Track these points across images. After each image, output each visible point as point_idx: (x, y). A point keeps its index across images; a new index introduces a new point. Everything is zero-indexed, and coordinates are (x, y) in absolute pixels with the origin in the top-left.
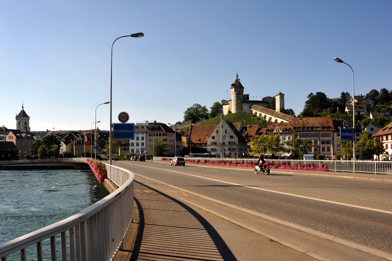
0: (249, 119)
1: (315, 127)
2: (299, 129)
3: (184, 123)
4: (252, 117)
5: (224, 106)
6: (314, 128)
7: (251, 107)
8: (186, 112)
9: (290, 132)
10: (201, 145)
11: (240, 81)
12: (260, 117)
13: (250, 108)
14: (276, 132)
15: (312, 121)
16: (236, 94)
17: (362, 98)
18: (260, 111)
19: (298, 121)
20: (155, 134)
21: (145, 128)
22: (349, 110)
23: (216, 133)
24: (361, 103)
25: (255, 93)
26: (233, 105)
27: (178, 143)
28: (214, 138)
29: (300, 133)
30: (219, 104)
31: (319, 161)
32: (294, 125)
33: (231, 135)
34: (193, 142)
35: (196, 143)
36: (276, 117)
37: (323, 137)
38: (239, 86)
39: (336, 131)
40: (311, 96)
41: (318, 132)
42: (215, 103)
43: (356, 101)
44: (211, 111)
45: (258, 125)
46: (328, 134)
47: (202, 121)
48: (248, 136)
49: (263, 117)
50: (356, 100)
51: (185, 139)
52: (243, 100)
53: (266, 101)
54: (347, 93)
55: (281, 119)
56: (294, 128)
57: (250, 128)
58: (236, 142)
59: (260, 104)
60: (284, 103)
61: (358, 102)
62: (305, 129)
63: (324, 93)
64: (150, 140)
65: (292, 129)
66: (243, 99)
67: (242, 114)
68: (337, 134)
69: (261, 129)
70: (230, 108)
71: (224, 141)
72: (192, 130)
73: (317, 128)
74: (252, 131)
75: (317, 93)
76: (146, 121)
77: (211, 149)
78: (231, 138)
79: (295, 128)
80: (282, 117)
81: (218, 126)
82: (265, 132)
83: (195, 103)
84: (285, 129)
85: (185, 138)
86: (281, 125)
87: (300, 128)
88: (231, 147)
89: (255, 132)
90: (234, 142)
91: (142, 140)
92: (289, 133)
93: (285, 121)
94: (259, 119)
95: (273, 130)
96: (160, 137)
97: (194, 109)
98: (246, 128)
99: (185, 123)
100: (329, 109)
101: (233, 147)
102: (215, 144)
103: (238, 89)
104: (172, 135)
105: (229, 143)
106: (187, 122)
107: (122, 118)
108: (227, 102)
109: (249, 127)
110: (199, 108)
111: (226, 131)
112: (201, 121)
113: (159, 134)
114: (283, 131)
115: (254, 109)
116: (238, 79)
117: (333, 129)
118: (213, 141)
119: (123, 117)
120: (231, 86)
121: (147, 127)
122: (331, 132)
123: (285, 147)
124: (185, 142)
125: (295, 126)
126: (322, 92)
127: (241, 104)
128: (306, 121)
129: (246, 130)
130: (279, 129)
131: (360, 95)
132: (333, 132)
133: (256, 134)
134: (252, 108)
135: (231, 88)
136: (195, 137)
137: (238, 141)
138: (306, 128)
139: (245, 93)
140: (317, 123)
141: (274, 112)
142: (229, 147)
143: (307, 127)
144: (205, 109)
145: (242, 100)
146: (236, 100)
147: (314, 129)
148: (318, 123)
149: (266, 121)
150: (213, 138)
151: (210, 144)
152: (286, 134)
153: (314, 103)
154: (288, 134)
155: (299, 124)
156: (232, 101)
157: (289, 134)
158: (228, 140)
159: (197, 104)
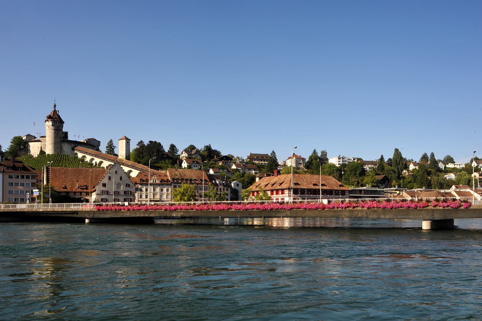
4: (81, 162)
5: (31, 144)
6: (193, 180)
13: (73, 149)
14: (152, 182)
16: (54, 130)
18: (93, 156)
23: (108, 180)
25: (76, 132)
29: (179, 185)
33: (126, 183)
35: (61, 191)
43: (187, 155)
50: (186, 153)
52: (63, 139)
60: (130, 150)
66: (61, 137)
71: (118, 190)
73: (195, 181)
77: (101, 199)
79: (174, 179)
80: (131, 166)
88: (128, 197)
90: (131, 192)
92: (168, 185)
96: (23, 179)
101: (129, 197)
103: (57, 123)
105: (125, 192)
111: (121, 178)
113: (27, 176)
114: (160, 182)
118: (104, 189)
123: (163, 200)
127: (61, 143)
130: (156, 180)
134: (76, 150)
139: (64, 130)
141: (117, 158)
142: (125, 197)
143: (186, 179)
146: (54, 137)
147: (193, 182)
150: (104, 185)
152: (165, 185)
154: (167, 185)
155: (176, 175)
157: (168, 185)
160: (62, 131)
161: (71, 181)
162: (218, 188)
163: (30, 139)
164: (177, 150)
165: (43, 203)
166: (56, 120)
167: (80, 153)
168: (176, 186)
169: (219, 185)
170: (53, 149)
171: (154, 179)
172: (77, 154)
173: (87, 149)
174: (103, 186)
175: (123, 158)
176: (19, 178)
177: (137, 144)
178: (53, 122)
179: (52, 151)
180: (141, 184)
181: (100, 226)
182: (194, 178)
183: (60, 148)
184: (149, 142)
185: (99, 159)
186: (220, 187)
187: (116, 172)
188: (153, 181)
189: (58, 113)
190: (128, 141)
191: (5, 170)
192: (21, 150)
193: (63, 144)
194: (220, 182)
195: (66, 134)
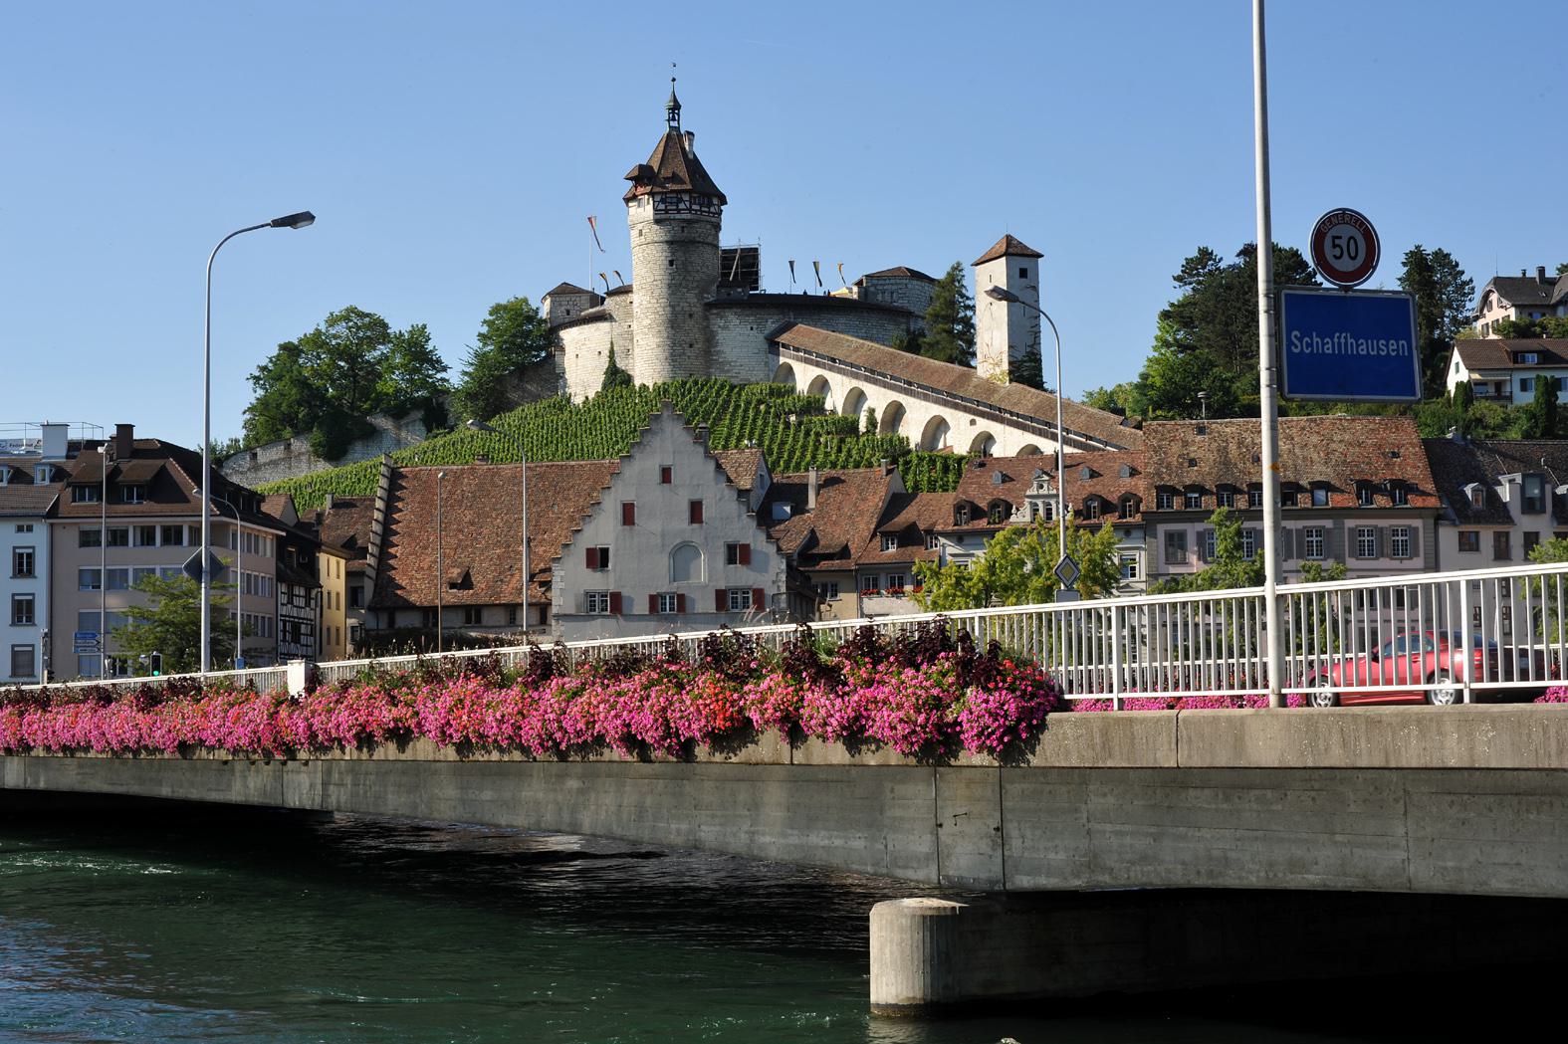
0: (775, 433)
1: (1304, 482)
3: (255, 456)
5: (568, 336)
6: (1300, 489)
8: (263, 369)
9: (1129, 519)
10: (479, 620)
11: (694, 149)
12: (851, 417)
13: (773, 346)
14: (1028, 519)
16: (665, 247)
17: (1549, 295)
18: (856, 376)
19: (1186, 444)
20: (131, 525)
21: (42, 479)
22: (1476, 376)
23: (620, 528)
24: (1544, 328)
26: (647, 322)
27: (296, 601)
30: (531, 317)
31: (1454, 586)
33: (730, 540)
34: (413, 598)
36: (977, 419)
38: (689, 187)
39: (1454, 517)
40: (1198, 275)
41: (1328, 524)
42: (497, 310)
43: (1512, 314)
44: (470, 369)
45: (889, 472)
46: (1395, 533)
47: (398, 443)
48: (815, 551)
49: (879, 416)
50: (1505, 302)
51: (338, 577)
53: (887, 297)
54: (1442, 257)
55: (1020, 432)
56: (1160, 489)
57: (830, 492)
58: (770, 591)
61: (1527, 319)
64: (88, 579)
65: (1149, 503)
66: (715, 284)
67: (718, 395)
68: (1461, 534)
69: (914, 496)
70: (619, 348)
72: (400, 505)
73: (1321, 494)
76: (46, 426)
78: (731, 560)
79: (1165, 492)
80: (1032, 419)
81: (631, 471)
82: (944, 520)
83: (338, 308)
84: (1092, 497)
85: (338, 563)
87: (1202, 490)
89: (866, 524)
90: (759, 594)
91: (14, 576)
93: (1048, 447)
94: (848, 428)
97: (339, 352)
98: (796, 495)
99: (263, 456)
103: (682, 206)
104: (257, 537)
105: (721, 597)
106: (276, 452)
107: (1337, 252)
108: (596, 300)
109: (819, 488)
110: (372, 343)
111: (696, 511)
112: (387, 443)
113: (166, 530)
115: (807, 361)
116: (677, 129)
117: (1433, 502)
118: (596, 581)
119: (1343, 243)
120: (630, 184)
121: (58, 474)
122: (1417, 523)
124: (338, 594)
125: (1167, 478)
128: (1240, 444)
129: (800, 508)
131: (1533, 273)
133: (878, 538)
135: (627, 200)
137: (787, 587)
138: (1241, 492)
139: (730, 238)
141: (964, 379)
144: (417, 351)
145: (714, 288)
146: (670, 286)
147: (1304, 502)
149: (903, 442)
150: (598, 559)
151: (573, 611)
153: (1227, 324)
155: (1192, 463)
156: (636, 297)
159: (362, 315)
160: (716, 247)
161: (497, 544)
162: (1507, 534)
163: (568, 312)
164: (1465, 283)
165: (1258, 579)
166: (680, 188)
167: (803, 365)
168: (1182, 535)
169: (1515, 511)
171: (1038, 497)
172: (790, 369)
173: (849, 343)
175: (998, 371)
176: (154, 544)
178: (663, 201)
179: (659, 368)
180: (959, 538)
182: (1321, 472)
184: (1238, 255)
185: (883, 389)
186: (1527, 523)
187: (666, 475)
188: (1035, 511)
189: (691, 145)
190: (1025, 263)
191: (69, 505)
192: (523, 371)
193: (717, 323)
194: (1523, 488)
195: (749, 259)
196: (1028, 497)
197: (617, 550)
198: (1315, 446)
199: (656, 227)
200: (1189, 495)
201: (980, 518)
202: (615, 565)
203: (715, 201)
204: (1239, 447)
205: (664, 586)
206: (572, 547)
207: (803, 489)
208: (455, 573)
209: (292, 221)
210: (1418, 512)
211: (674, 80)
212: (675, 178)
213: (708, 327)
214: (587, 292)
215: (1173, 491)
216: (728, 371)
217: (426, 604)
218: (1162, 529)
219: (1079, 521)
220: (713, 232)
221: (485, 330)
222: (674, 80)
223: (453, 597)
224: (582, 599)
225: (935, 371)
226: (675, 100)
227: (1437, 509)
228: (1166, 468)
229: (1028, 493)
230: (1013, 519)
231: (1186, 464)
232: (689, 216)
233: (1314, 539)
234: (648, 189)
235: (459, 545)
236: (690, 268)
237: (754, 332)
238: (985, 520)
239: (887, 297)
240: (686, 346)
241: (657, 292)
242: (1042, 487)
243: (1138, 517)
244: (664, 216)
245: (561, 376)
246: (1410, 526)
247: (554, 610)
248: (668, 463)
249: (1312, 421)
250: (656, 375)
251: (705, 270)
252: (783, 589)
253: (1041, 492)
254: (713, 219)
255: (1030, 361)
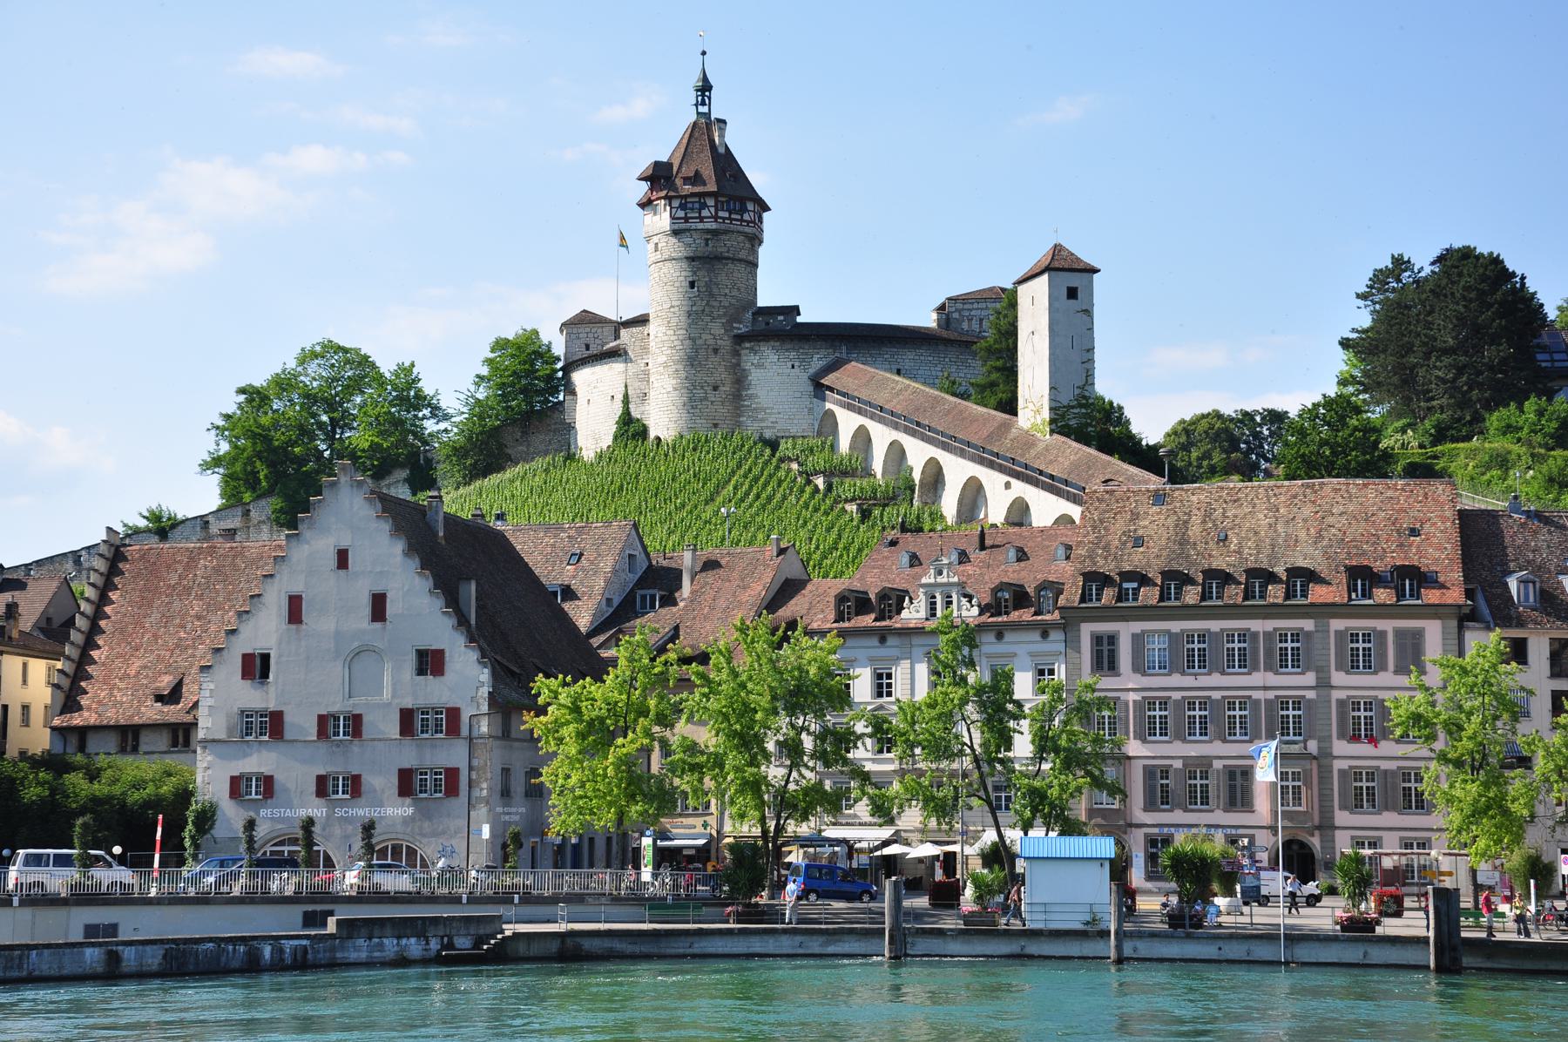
1: (1280, 570)
2: (1136, 591)
5: (580, 377)
7: (825, 381)
8: (227, 417)
9: (1047, 617)
13: (819, 389)
14: (923, 614)
15: (1262, 519)
16: (685, 265)
18: (896, 427)
19: (1135, 516)
23: (284, 626)
28: (265, 674)
29: (1137, 627)
32: (1091, 557)
35: (137, 720)
36: (1014, 482)
37: (1354, 666)
39: (1489, 618)
41: (1308, 625)
57: (709, 576)
59: (908, 357)
60: (1091, 350)
62: (1275, 593)
63: (1496, 261)
65: (1070, 596)
70: (634, 394)
71: (356, 705)
74: (722, 603)
75: (1440, 260)
78: (421, 671)
79: (1095, 580)
80: (1066, 483)
83: (311, 340)
86: (983, 547)
87: (1144, 580)
95: (893, 601)
97: (310, 398)
100: (1540, 413)
102: (274, 725)
103: (705, 213)
105: (408, 720)
110: (355, 385)
115: (850, 407)
120: (645, 186)
125: (1101, 562)
126: (1483, 248)
128: (1208, 515)
129: (669, 601)
132: (1454, 623)
134: (831, 389)
136: (137, 664)
138: (1192, 581)
140: (1302, 535)
141: (1005, 427)
143: (1210, 574)
146: (689, 314)
148: (1320, 537)
150: (257, 667)
151: (222, 736)
154: (875, 641)
155: (1139, 542)
156: (654, 328)
157: (883, 640)
158: (393, 687)
163: (587, 347)
166: (709, 198)
170: (679, 403)
171: (936, 585)
174: (247, 673)
177: (1363, 289)
178: (682, 207)
179: (675, 415)
181: (578, 973)
183: (726, 388)
187: (342, 559)
190: (1074, 280)
193: (749, 360)
196: (923, 586)
197: (280, 656)
198: (1305, 520)
199: (673, 240)
200: (1125, 585)
201: (867, 613)
202: (276, 678)
203: (750, 206)
204: (1204, 522)
205: (336, 704)
206: (225, 653)
207: (678, 574)
208: (165, 683)
209: (623, 238)
210: (1433, 610)
211: (704, 53)
212: (697, 179)
213: (738, 364)
214: (611, 322)
215: (1106, 580)
216: (762, 420)
217: (122, 722)
218: (1087, 630)
219: (985, 618)
220: (748, 245)
221: (485, 371)
222: (704, 53)
223: (153, 712)
224: (236, 718)
225: (975, 419)
226: (705, 79)
227: (1459, 606)
228: (1104, 549)
229: (924, 581)
230: (905, 614)
231: (1130, 545)
232: (714, 226)
233: (1289, 645)
234: (663, 193)
235: (177, 646)
236: (715, 291)
237: (797, 370)
238: (873, 616)
239: (975, 326)
240: (709, 389)
241: (674, 321)
242: (940, 573)
243: (1057, 615)
244: (683, 226)
245: (570, 428)
246: (1374, 630)
247: (201, 734)
248: (344, 544)
249: (1308, 486)
250: (672, 425)
251: (735, 293)
252: (485, 708)
253: (940, 580)
254: (747, 230)
255: (1080, 406)
